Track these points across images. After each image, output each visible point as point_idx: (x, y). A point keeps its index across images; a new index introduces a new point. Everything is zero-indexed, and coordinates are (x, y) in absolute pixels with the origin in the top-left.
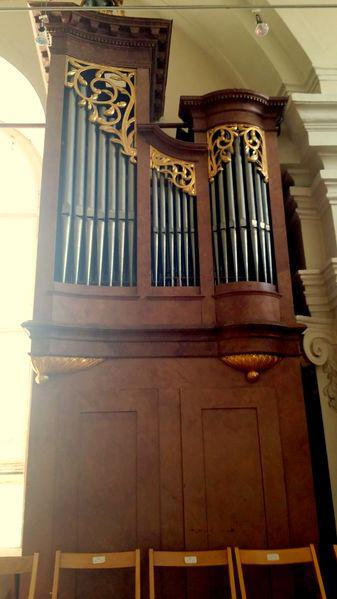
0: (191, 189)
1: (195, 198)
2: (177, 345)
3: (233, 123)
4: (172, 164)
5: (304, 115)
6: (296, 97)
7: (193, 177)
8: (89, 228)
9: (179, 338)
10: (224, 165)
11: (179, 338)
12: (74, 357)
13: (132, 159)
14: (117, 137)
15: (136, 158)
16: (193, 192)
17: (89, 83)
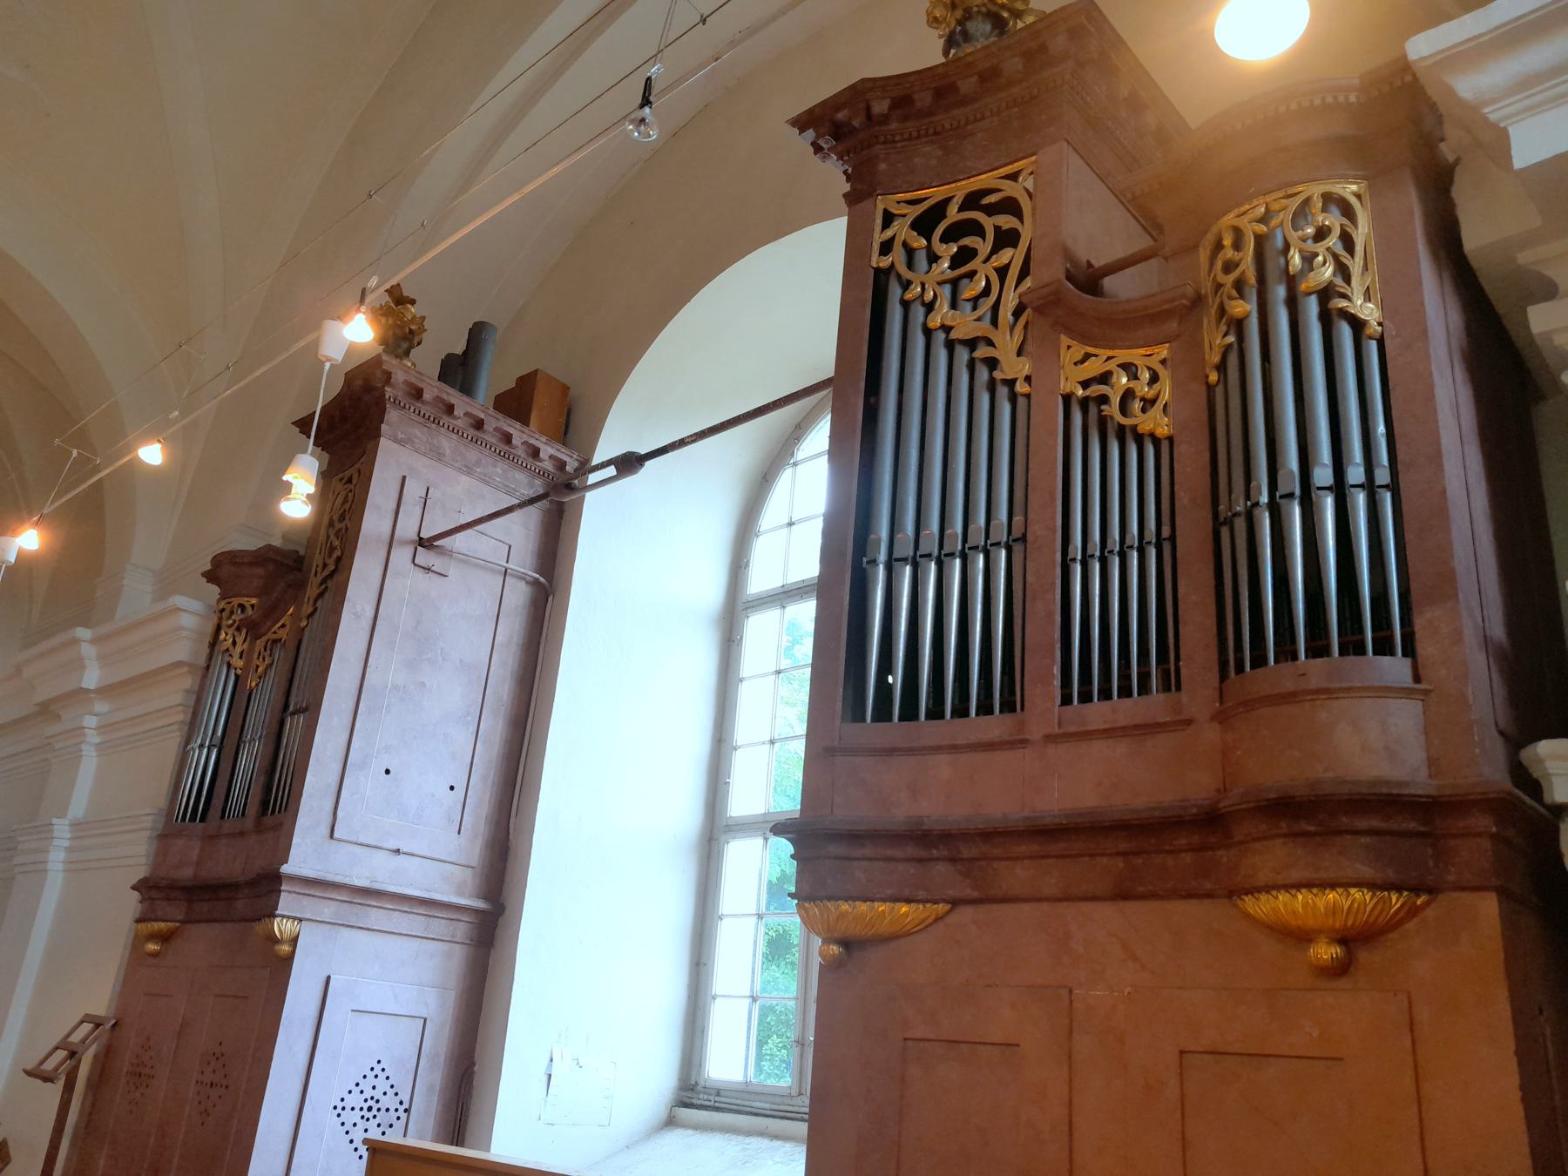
0: (1156, 422)
1: (1170, 439)
2: (1120, 863)
3: (1250, 198)
4: (1112, 365)
5: (1469, 86)
6: (1422, 47)
7: (1166, 391)
8: (926, 583)
9: (1123, 846)
10: (1239, 325)
11: (1123, 846)
12: (884, 900)
13: (1021, 387)
14: (990, 343)
15: (1028, 379)
16: (1163, 431)
17: (929, 240)
